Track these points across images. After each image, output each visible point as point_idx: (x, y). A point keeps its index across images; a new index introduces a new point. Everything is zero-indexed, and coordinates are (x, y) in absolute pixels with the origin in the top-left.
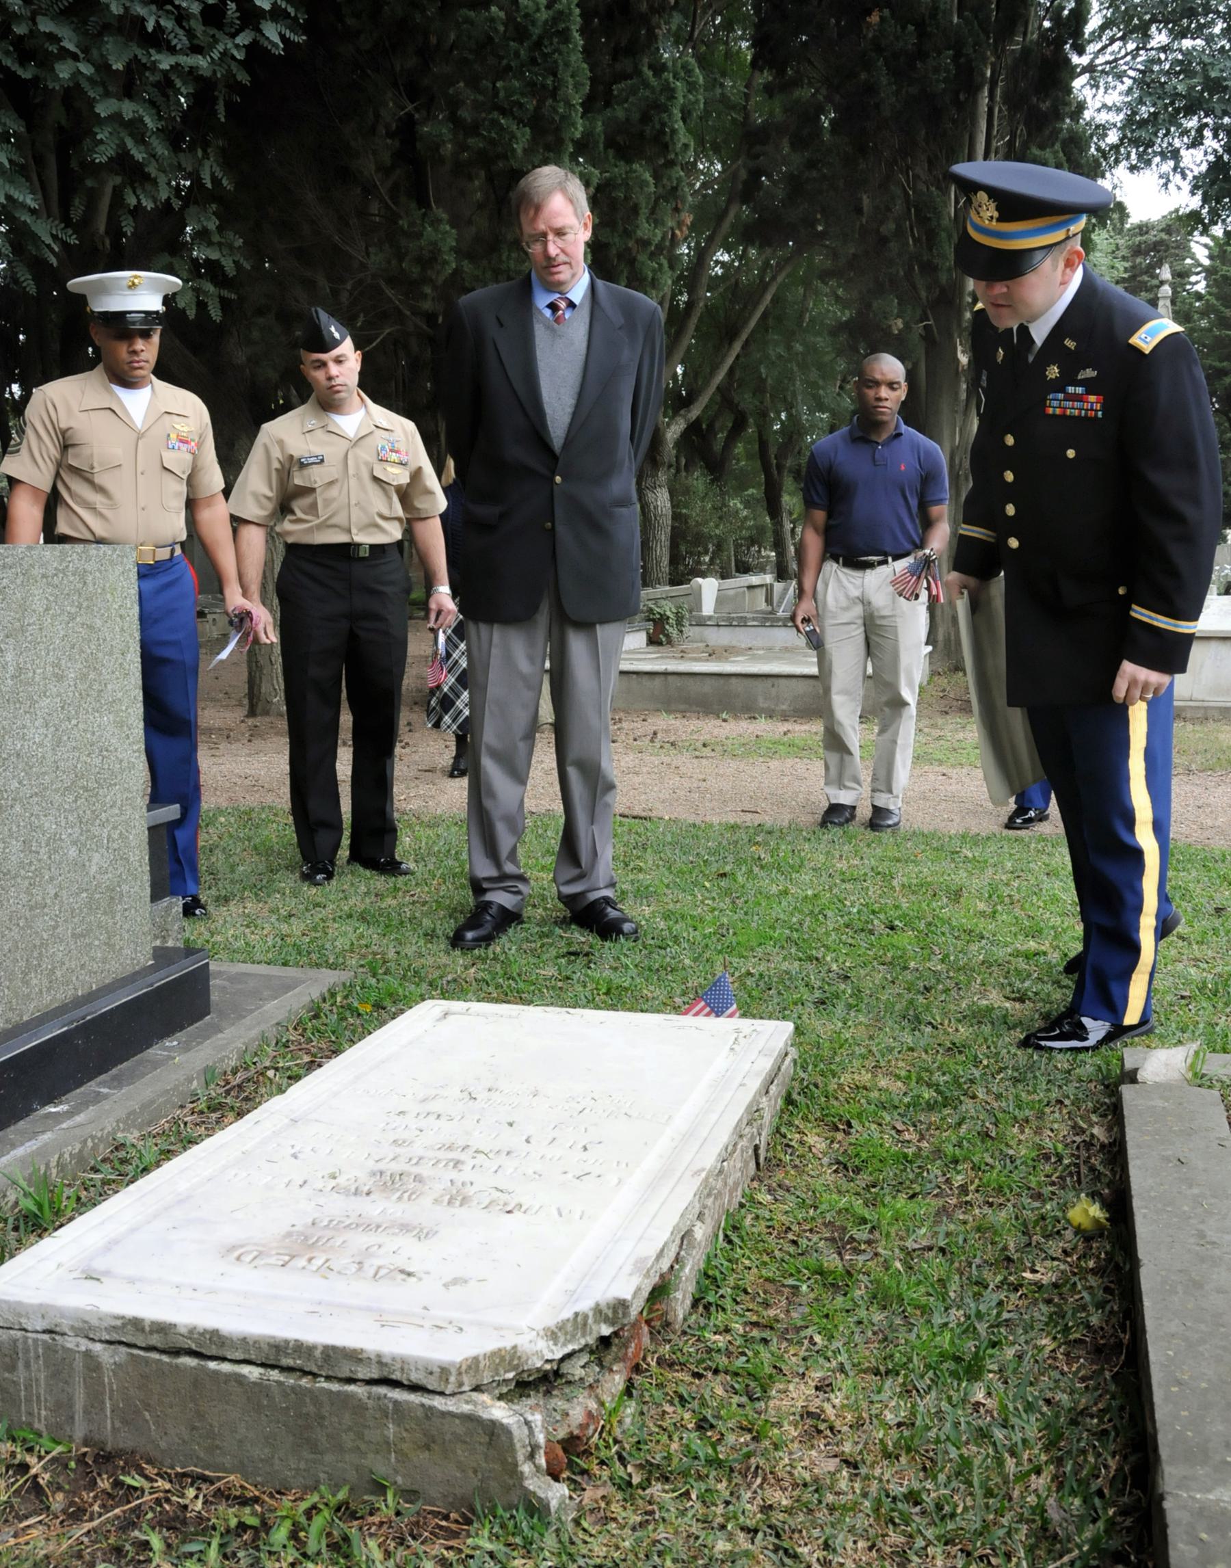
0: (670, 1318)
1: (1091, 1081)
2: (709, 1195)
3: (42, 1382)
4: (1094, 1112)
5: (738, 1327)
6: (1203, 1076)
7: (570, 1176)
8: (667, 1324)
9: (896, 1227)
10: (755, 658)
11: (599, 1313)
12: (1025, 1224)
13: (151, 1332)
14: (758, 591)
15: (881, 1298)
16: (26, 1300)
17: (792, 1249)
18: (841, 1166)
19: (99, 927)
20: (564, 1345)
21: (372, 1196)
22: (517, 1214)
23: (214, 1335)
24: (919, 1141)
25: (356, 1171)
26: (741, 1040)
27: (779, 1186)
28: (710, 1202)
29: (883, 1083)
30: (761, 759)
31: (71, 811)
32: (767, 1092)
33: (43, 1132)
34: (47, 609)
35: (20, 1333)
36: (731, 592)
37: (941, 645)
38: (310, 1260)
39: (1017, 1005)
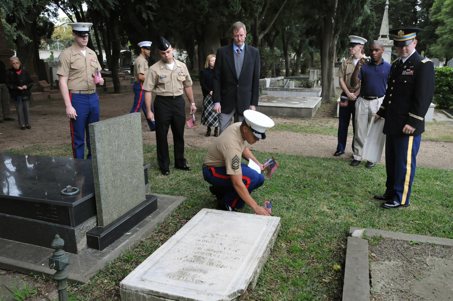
0: (252, 288)
1: (343, 233)
2: (261, 262)
3: (135, 299)
4: (343, 240)
5: (265, 290)
6: (366, 236)
7: (233, 258)
8: (251, 290)
9: (298, 267)
10: (279, 101)
11: (238, 292)
12: (324, 268)
13: (155, 293)
14: (280, 81)
15: (294, 284)
16: (132, 285)
17: (277, 272)
18: (288, 252)
19: (135, 194)
20: (232, 298)
21: (194, 262)
22: (223, 268)
23: (167, 294)
24: (305, 245)
25: (190, 257)
26: (269, 222)
27: (275, 256)
28: (260, 264)
29: (299, 230)
30: (279, 131)
31: (129, 172)
32: (274, 235)
33: (127, 239)
34: (123, 131)
35: (131, 291)
36: (274, 82)
37: (324, 97)
38: (183, 278)
39: (330, 211)
